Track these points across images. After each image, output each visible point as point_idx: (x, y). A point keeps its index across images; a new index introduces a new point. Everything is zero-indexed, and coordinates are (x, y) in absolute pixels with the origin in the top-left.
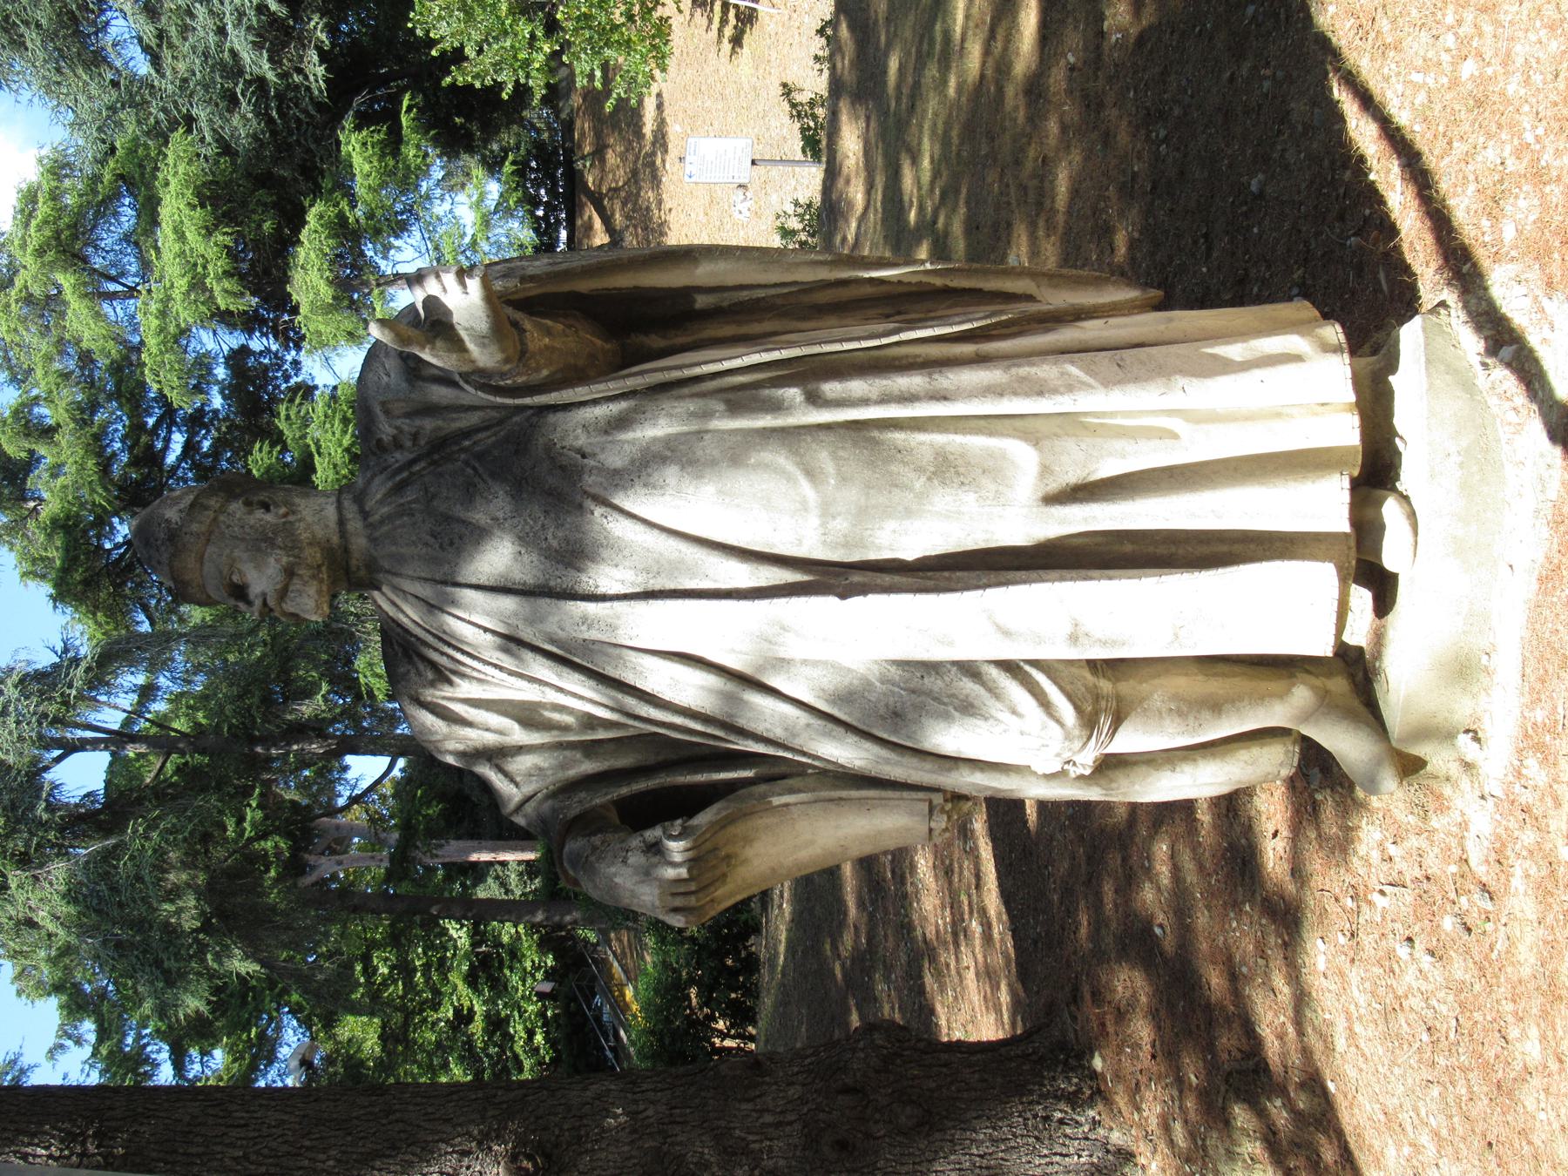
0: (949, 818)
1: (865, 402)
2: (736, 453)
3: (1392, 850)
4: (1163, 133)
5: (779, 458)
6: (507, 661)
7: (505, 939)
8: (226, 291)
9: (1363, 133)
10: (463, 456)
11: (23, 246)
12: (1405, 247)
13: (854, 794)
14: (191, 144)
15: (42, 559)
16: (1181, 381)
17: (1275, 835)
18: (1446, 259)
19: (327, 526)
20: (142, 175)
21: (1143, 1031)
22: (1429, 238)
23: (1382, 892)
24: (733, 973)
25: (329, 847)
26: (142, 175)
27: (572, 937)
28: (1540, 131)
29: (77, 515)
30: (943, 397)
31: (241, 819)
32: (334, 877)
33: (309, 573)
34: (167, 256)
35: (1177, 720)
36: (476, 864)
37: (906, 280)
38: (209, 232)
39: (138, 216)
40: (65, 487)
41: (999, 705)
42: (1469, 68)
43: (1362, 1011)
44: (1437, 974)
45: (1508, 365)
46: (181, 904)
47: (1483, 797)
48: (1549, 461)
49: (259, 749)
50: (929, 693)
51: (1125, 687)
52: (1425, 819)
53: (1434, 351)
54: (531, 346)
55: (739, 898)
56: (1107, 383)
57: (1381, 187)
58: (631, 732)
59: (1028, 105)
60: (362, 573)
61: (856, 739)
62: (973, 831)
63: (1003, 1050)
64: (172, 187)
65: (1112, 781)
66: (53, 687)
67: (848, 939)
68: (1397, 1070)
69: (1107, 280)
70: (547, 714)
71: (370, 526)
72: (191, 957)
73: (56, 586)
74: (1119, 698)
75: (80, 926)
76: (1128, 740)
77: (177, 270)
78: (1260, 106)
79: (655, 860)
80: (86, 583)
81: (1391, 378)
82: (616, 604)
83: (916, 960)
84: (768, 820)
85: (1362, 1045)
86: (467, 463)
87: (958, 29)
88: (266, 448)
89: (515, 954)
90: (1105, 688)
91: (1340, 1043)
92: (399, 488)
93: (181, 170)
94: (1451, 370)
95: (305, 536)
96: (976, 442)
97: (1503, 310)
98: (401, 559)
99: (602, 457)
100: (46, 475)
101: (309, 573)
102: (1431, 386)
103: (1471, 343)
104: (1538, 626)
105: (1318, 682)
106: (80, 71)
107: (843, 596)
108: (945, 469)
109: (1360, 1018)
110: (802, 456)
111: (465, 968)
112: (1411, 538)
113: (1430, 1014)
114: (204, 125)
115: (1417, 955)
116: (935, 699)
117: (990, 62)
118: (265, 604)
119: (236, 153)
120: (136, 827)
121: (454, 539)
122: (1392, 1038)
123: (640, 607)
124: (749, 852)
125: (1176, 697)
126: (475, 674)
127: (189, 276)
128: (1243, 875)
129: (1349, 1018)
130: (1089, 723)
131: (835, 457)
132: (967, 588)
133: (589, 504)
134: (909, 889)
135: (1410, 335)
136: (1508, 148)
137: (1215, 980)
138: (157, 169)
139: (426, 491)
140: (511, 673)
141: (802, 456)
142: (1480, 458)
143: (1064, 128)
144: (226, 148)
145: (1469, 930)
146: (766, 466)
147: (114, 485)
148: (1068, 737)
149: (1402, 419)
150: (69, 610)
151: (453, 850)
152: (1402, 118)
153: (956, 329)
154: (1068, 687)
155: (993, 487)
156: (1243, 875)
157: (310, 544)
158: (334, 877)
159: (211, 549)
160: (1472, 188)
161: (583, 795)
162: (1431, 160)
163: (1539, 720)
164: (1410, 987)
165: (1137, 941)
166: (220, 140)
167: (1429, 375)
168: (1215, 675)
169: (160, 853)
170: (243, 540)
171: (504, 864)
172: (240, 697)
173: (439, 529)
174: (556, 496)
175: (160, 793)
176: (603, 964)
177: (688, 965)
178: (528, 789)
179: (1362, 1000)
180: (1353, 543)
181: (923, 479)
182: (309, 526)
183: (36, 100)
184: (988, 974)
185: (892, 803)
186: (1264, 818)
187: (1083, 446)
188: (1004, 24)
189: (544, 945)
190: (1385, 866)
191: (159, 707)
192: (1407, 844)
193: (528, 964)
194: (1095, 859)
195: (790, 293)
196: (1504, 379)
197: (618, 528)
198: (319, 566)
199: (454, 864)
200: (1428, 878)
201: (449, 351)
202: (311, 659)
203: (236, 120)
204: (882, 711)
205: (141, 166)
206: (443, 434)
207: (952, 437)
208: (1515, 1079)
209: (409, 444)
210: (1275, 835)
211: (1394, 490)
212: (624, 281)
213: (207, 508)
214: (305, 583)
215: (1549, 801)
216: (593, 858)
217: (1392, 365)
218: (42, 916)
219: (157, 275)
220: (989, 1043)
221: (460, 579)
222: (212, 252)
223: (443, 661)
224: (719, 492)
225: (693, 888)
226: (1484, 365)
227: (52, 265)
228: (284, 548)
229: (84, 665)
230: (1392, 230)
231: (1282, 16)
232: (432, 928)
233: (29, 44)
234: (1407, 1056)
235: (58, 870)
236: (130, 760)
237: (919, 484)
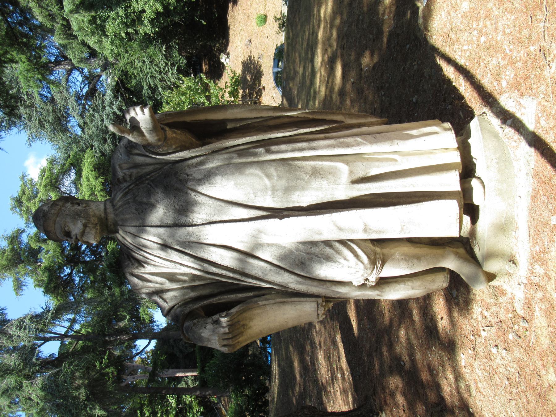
0: (325, 309)
1: (286, 151)
2: (240, 168)
3: (486, 314)
4: (383, 93)
5: (256, 171)
6: (162, 254)
7: (188, 402)
8: (101, 195)
9: (449, 71)
10: (147, 182)
11: (40, 186)
12: (468, 102)
13: (289, 300)
14: (92, 153)
15: (41, 280)
16: (397, 142)
17: (442, 319)
18: (483, 99)
19: (100, 211)
20: (78, 163)
21: (400, 399)
22: (476, 95)
23: (484, 330)
24: (261, 406)
25: (130, 373)
26: (78, 163)
27: (209, 401)
28: (511, 47)
29: (53, 266)
30: (314, 149)
31: (101, 363)
32: (132, 383)
33: (92, 226)
34: (84, 186)
35: (405, 263)
36: (178, 377)
37: (299, 116)
38: (97, 178)
39: (76, 175)
40: (50, 257)
41: (339, 257)
42: (483, 39)
43: (481, 378)
44: (509, 357)
45: (510, 126)
46: (80, 392)
47: (519, 284)
48: (530, 154)
49: (107, 338)
50: (314, 254)
51: (386, 251)
52: (497, 300)
53: (484, 129)
54: (168, 136)
55: (249, 342)
56: (371, 143)
57: (457, 86)
58: (208, 281)
59: (340, 99)
60: (112, 227)
61: (288, 274)
62: (336, 342)
63: (350, 414)
64: (86, 166)
65: (383, 289)
66: (41, 320)
67: (297, 388)
68: (497, 398)
69: (368, 116)
70: (178, 277)
71: (115, 210)
72: (82, 409)
73: (45, 288)
74: (383, 255)
75: (45, 399)
76: (389, 271)
77: (87, 190)
78: (414, 75)
79: (217, 326)
80: (55, 287)
81: (469, 141)
82: (199, 227)
83: (321, 390)
84: (258, 311)
85: (482, 391)
86: (148, 184)
87: (318, 87)
88: (112, 243)
89: (191, 407)
90: (378, 248)
91: (474, 392)
92: (125, 195)
93: (89, 160)
94: (490, 132)
95: (91, 213)
96: (326, 164)
97: (506, 108)
98: (124, 220)
99: (194, 175)
100: (44, 254)
101: (92, 226)
102: (483, 137)
103: (495, 122)
104: (533, 215)
105: (454, 250)
106: (60, 134)
107: (281, 219)
108: (316, 173)
109: (480, 381)
110: (264, 170)
111: (174, 413)
112: (483, 190)
113: (508, 373)
114: (96, 147)
115: (500, 351)
116: (316, 256)
117: (328, 90)
118: (76, 238)
119: (106, 156)
120: (65, 365)
121: (143, 209)
122: (494, 386)
123: (208, 227)
124: (251, 324)
125: (404, 254)
126: (154, 263)
127: (90, 192)
128: (431, 337)
129: (476, 382)
130: (373, 263)
131: (276, 170)
132: (326, 214)
133: (190, 192)
134: (317, 367)
135: (474, 125)
136: (500, 58)
137: (425, 376)
138: (82, 161)
139: (134, 195)
140: (164, 259)
141: (264, 170)
142: (504, 161)
143: (352, 102)
144: (103, 154)
145: (520, 337)
146: (252, 174)
147: (65, 256)
148: (366, 268)
149: (475, 152)
150: (49, 296)
151: (170, 373)
152: (462, 62)
153: (317, 129)
154: (365, 250)
155: (333, 179)
156: (431, 337)
157: (93, 216)
158: (132, 383)
159: (58, 219)
160: (489, 75)
161: (191, 305)
162: (473, 72)
163: (538, 250)
164: (499, 364)
165: (397, 367)
166: (101, 152)
167: (482, 134)
168: (417, 247)
169: (73, 373)
170: (70, 215)
171: (187, 377)
172: (101, 321)
173: (138, 207)
174: (176, 185)
175: (75, 353)
176: (219, 409)
177: (245, 404)
178: (171, 304)
179: (480, 373)
180: (462, 196)
181: (308, 176)
182: (93, 210)
183: (47, 142)
184: (344, 392)
185: (303, 303)
186: (437, 314)
187: (364, 164)
188: (331, 77)
189: (200, 404)
190: (484, 320)
191: (77, 327)
192: (491, 310)
193: (195, 411)
194: (379, 341)
195: (260, 121)
196: (510, 131)
197: (200, 198)
198: (96, 224)
199: (171, 377)
200: (501, 321)
201: (138, 136)
202: (125, 308)
203: (106, 146)
204: (297, 262)
205: (77, 160)
206: (140, 174)
207: (318, 162)
208: (546, 391)
209: (128, 179)
210: (442, 319)
211: (474, 176)
212: (202, 117)
213: (57, 205)
214: (91, 230)
215: (546, 279)
216: (194, 328)
217: (469, 135)
218: (33, 397)
219: (80, 192)
220: (346, 412)
221: (145, 224)
222: (97, 184)
223: (141, 258)
224: (236, 184)
225: (231, 337)
226: (502, 128)
227: (49, 190)
228: (84, 217)
229: (51, 312)
230: (461, 98)
231: (418, 45)
232: (164, 399)
233: (46, 127)
234: (501, 391)
235: (39, 380)
236: (67, 345)
237: (306, 178)
